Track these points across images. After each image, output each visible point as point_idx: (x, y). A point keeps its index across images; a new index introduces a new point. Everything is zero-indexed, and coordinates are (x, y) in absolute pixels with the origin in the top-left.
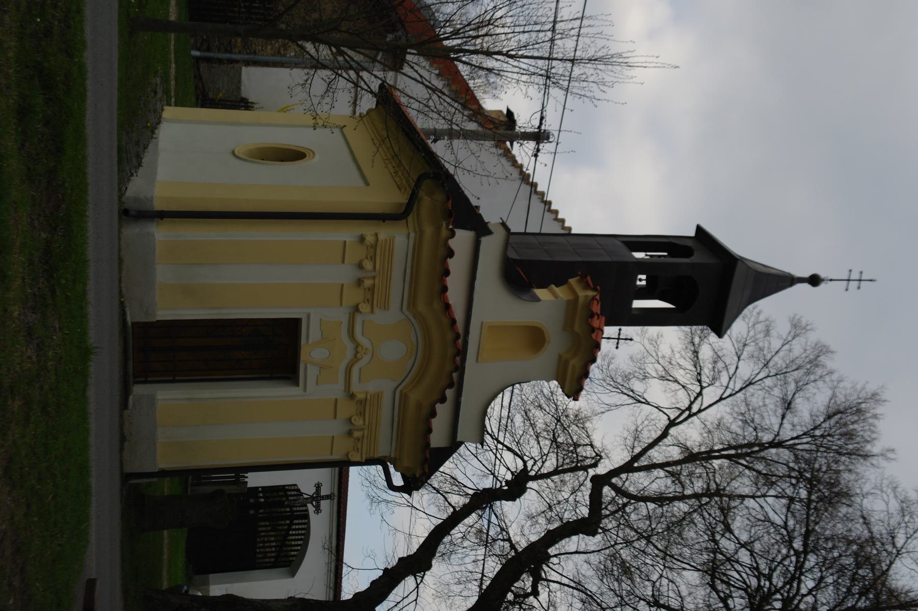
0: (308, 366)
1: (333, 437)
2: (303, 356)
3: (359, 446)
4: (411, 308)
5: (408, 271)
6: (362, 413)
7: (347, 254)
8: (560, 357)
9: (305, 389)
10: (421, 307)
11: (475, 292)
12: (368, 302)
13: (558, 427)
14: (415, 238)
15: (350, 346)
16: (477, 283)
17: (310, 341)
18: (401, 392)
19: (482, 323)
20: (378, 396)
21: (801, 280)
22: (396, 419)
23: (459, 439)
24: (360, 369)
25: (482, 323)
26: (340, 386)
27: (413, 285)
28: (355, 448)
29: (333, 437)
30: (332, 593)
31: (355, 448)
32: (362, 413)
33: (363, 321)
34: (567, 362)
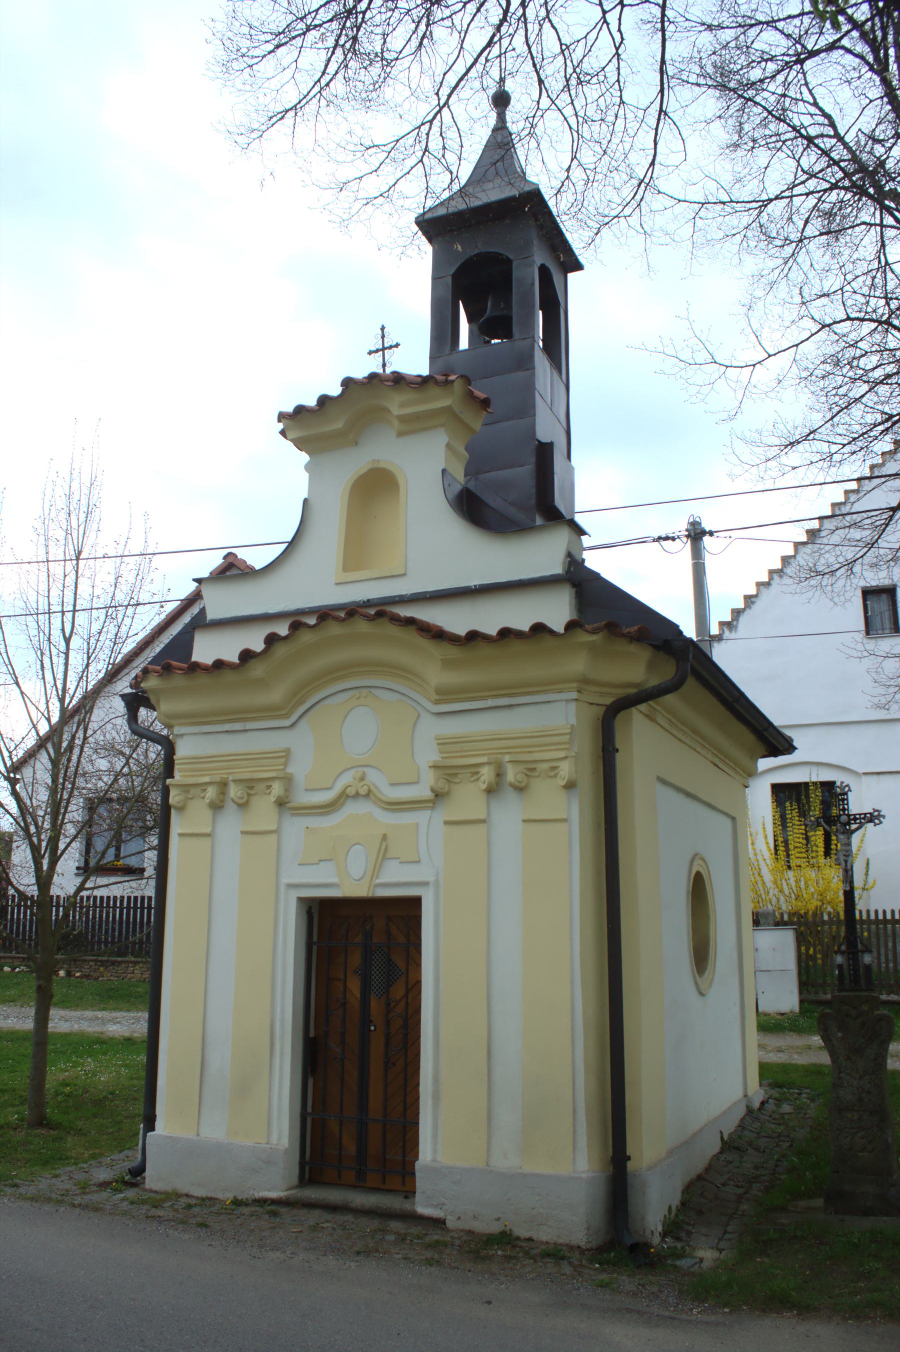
0: (378, 881)
1: (524, 821)
2: (359, 891)
3: (545, 766)
4: (284, 712)
5: (227, 727)
6: (473, 770)
7: (196, 831)
8: (400, 434)
9: (425, 884)
10: (275, 695)
11: (286, 609)
12: (478, 773)
13: (893, 382)
14: (182, 725)
15: (351, 809)
16: (272, 610)
17: (335, 880)
18: (437, 702)
19: (337, 584)
20: (444, 743)
21: (501, 118)
22: (490, 703)
23: (196, 584)
24: (392, 785)
25: (337, 584)
26: (421, 817)
27: (249, 716)
28: (552, 774)
29: (524, 821)
30: (83, 859)
31: (552, 774)
32: (473, 770)
33: (306, 790)
34: (403, 419)
